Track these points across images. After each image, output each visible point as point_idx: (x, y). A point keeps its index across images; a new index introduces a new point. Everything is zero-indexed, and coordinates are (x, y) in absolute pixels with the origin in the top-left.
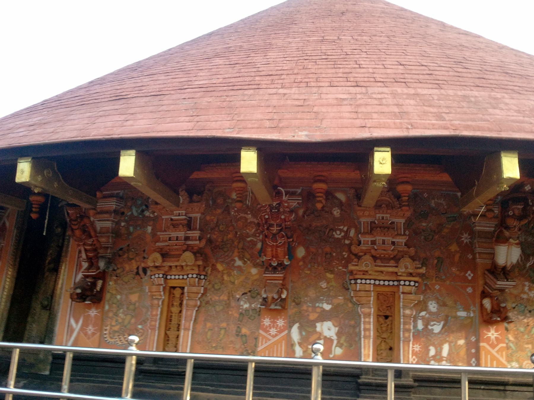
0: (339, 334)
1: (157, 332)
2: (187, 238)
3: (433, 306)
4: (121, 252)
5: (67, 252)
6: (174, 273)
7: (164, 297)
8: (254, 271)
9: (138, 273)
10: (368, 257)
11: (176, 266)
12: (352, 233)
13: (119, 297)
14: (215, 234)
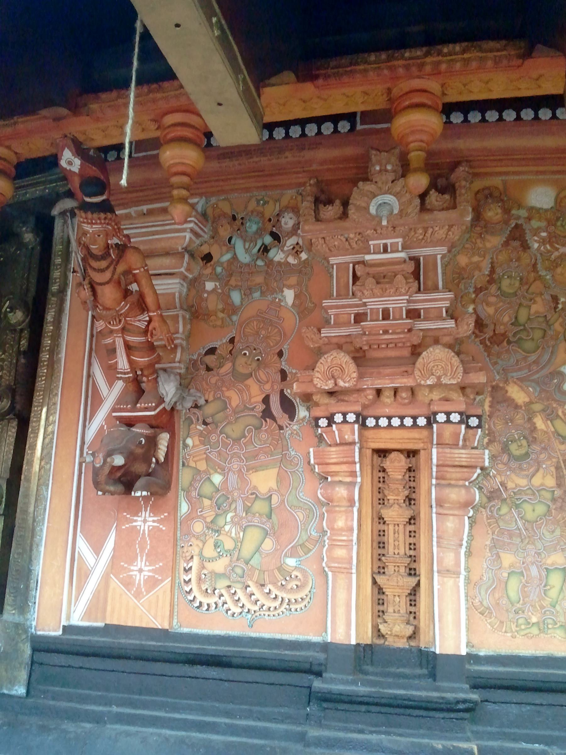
1: (354, 577)
2: (414, 314)
4: (210, 360)
5: (52, 364)
6: (387, 411)
7: (363, 479)
9: (267, 414)
11: (396, 391)
13: (217, 479)
14: (488, 304)
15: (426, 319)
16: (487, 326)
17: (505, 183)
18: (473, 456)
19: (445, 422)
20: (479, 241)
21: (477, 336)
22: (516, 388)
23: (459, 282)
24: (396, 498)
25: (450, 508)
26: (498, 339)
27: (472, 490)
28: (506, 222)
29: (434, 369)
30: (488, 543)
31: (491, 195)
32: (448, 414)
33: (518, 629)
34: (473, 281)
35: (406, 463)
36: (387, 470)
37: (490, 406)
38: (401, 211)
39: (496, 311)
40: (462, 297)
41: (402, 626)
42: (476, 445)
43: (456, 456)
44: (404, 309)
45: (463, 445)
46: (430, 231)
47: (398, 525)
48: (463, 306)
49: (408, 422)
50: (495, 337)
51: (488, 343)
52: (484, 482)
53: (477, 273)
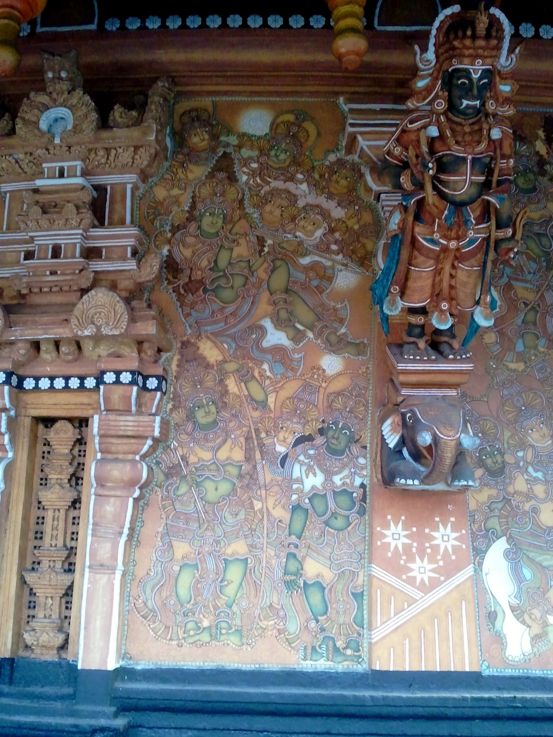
2: (91, 253)
6: (49, 370)
8: (331, 364)
11: (57, 344)
15: (108, 259)
16: (182, 271)
17: (215, 105)
18: (141, 424)
19: (114, 383)
20: (180, 171)
21: (169, 283)
22: (209, 344)
23: (154, 219)
24: (59, 476)
25: (112, 488)
26: (193, 286)
27: (139, 465)
28: (213, 150)
29: (96, 317)
30: (160, 529)
31: (198, 118)
32: (118, 373)
33: (186, 635)
34: (170, 218)
35: (74, 434)
36: (51, 444)
37: (178, 366)
38: (75, 127)
39: (194, 253)
40: (156, 237)
41: (52, 634)
42: (154, 411)
43: (122, 423)
44: (78, 245)
45: (137, 411)
46: (113, 152)
47: (59, 510)
48: (157, 246)
49: (74, 383)
50: (190, 285)
51: (182, 291)
52: (163, 456)
53: (175, 209)
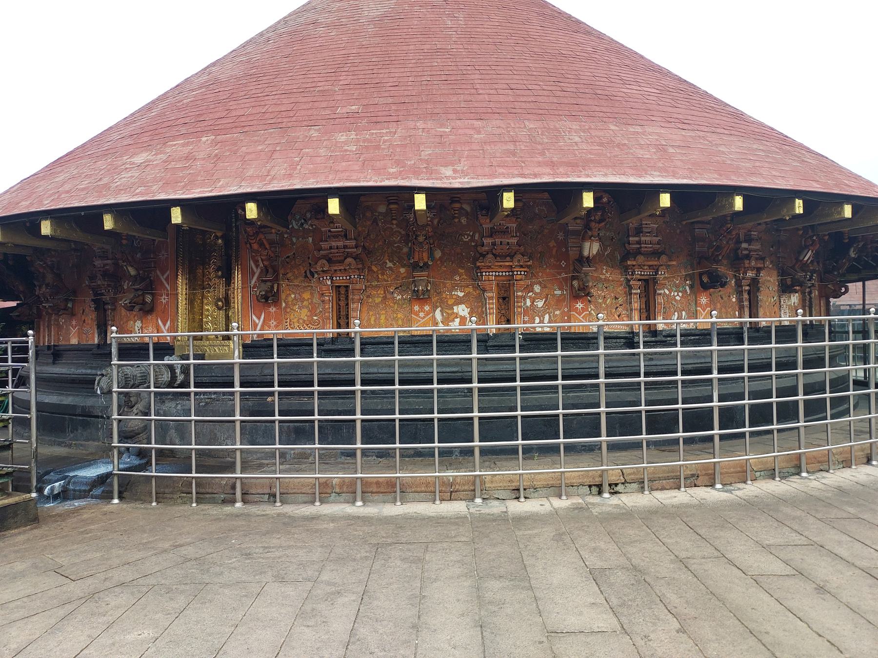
0: (471, 314)
2: (345, 247)
3: (537, 288)
8: (402, 270)
9: (306, 276)
10: (490, 256)
12: (477, 236)
13: (293, 296)
